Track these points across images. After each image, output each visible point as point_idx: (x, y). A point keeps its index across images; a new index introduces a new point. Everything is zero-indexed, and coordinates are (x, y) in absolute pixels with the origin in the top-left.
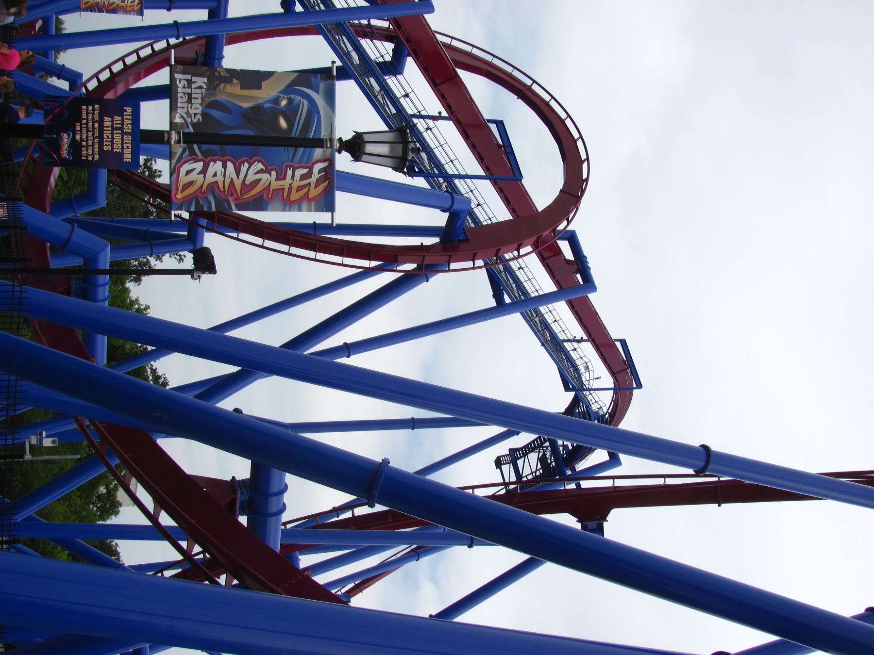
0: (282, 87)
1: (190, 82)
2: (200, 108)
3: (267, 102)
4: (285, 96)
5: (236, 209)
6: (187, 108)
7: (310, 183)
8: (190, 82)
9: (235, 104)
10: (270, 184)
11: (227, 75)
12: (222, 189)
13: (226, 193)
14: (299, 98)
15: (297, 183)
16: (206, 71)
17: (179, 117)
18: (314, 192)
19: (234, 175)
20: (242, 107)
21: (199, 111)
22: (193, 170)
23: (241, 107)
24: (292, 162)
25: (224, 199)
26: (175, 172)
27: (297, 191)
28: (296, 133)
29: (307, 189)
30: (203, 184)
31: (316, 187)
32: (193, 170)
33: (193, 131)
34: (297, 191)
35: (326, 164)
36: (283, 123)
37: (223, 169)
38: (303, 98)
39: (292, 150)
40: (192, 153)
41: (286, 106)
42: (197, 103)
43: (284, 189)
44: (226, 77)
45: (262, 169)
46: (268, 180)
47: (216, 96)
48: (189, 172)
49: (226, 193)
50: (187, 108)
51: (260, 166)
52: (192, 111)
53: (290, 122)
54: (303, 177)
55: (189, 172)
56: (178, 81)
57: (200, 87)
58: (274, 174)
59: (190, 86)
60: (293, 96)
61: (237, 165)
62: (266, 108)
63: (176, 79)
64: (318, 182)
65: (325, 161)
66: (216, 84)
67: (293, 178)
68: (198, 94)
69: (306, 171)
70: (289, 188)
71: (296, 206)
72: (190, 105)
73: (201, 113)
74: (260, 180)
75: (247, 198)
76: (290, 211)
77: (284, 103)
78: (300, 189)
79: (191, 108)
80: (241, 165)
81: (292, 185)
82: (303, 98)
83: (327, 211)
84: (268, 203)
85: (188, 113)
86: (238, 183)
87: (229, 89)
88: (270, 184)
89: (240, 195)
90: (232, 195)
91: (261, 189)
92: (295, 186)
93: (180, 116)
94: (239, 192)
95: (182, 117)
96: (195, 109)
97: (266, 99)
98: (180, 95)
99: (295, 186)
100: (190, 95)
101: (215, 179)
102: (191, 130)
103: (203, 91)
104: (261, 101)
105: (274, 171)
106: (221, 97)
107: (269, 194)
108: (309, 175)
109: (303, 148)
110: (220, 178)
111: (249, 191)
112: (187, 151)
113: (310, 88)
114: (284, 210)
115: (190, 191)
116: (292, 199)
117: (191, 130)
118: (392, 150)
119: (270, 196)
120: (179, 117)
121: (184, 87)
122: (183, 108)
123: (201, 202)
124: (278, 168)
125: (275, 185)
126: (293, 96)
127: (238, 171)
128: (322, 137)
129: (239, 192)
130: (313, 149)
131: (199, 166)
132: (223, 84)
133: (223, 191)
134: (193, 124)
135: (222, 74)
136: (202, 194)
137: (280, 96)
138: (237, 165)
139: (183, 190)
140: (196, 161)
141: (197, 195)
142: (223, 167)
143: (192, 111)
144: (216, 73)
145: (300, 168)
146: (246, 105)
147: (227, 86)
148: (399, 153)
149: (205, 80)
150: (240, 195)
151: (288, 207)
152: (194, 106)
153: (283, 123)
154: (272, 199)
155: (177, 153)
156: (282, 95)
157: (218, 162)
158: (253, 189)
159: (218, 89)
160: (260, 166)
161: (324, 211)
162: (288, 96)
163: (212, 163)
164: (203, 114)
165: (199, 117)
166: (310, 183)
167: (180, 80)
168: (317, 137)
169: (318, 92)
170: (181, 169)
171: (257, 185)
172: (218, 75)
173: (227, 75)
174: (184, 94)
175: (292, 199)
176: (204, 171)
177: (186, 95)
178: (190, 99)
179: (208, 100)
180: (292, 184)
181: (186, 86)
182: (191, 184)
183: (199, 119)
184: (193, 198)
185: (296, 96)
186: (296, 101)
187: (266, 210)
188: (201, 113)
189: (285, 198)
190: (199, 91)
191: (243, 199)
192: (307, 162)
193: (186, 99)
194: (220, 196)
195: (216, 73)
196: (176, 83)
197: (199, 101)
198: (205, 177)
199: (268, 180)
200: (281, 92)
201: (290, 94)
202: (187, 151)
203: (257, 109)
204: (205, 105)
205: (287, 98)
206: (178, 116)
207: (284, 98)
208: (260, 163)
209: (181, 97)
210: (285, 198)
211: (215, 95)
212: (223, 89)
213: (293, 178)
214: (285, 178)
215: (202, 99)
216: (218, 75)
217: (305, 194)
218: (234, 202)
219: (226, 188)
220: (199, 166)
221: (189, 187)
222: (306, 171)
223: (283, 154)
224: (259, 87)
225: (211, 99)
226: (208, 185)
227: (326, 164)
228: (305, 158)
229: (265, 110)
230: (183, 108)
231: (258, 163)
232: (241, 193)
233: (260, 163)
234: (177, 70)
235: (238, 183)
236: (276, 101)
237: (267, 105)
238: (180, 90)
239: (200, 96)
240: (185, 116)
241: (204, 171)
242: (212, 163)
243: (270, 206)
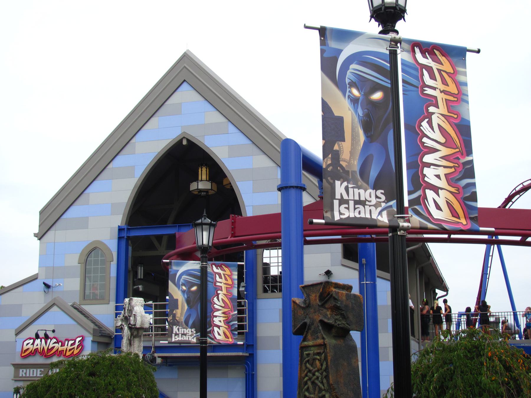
0: (339, 93)
1: (176, 334)
2: (188, 330)
3: (184, 296)
4: (348, 90)
5: (471, 155)
6: (188, 336)
7: (223, 274)
8: (176, 334)
9: (186, 312)
10: (442, 115)
11: (330, 156)
12: (453, 170)
13: (456, 165)
14: (181, 280)
15: (223, 280)
16: (328, 181)
17: (193, 339)
18: (447, 66)
19: (220, 312)
20: (187, 309)
21: (190, 330)
22: (218, 332)
23: (365, 142)
24: (418, 87)
25: (463, 168)
26: (441, 225)
27: (227, 281)
28: (197, 281)
29: (226, 276)
30: (225, 328)
31: (442, 64)
32: (218, 332)
33: (395, 201)
34: (227, 281)
35: (417, 50)
36: (194, 288)
37: (432, 167)
38: (348, 69)
39: (209, 283)
40: (210, 332)
41: (185, 286)
42: (186, 331)
43: (446, 100)
44: (332, 159)
45: (427, 122)
46: (438, 117)
47: (355, 172)
48: (219, 334)
49: (456, 165)
50: (188, 336)
51: (425, 124)
52: (190, 333)
53: (193, 285)
54: (220, 277)
55: (219, 334)
56: (176, 340)
57: (178, 329)
58: (219, 292)
59: (178, 334)
60: (181, 283)
61: (425, 150)
62: (187, 297)
63: (175, 341)
64: (223, 270)
65: (414, 52)
66: (341, 171)
67: (221, 283)
68: (182, 331)
69: (217, 276)
70: (445, 94)
71: (463, 88)
72: (367, 203)
73: (375, 190)
74: (439, 126)
75: (460, 142)
76: (467, 96)
77: (184, 288)
78: (226, 279)
79: (188, 334)
80: (426, 146)
81: (441, 90)
82: (181, 278)
83: (464, 56)
84: (463, 119)
85: (191, 336)
86: (445, 151)
87: (345, 155)
88: (442, 115)
89: (458, 150)
90: (458, 159)
91: (449, 125)
92: (225, 282)
93: (193, 339)
94: (228, 310)
95: (193, 338)
96: (189, 332)
97: (183, 297)
98: (182, 339)
99: (225, 282)
100: (182, 334)
101: (443, 177)
102: (199, 334)
103: (180, 328)
104: (184, 299)
105: (429, 109)
106: (183, 319)
107: (229, 295)
108: (430, 70)
109: (208, 278)
110: (442, 172)
111: (453, 139)
112: (416, 207)
113: (176, 274)
114: (467, 102)
115: (228, 334)
116: (231, 283)
117: (199, 334)
118: (206, 230)
119: (456, 116)
120: (193, 339)
121: (348, 208)
122: (189, 338)
123: (233, 328)
124: (426, 104)
125: (224, 291)
126: (181, 283)
127: (218, 310)
128: (388, 52)
129: (228, 310)
130: (208, 272)
131: (216, 329)
132: (176, 318)
133: (455, 169)
134: (388, 200)
135: (329, 162)
136: (459, 193)
137: (181, 290)
138: (425, 150)
139: (228, 338)
140: (213, 330)
141: (461, 198)
142: (429, 167)
143: (190, 333)
144: (171, 321)
145: (216, 279)
146: (186, 307)
147: (342, 157)
148: (208, 227)
149: (174, 327)
150: (458, 150)
151: (464, 97)
152: (188, 332)
153: (194, 288)
154: (458, 114)
155: (420, 222)
156: (180, 289)
157: (214, 320)
158: (227, 303)
159: (179, 321)
160: (425, 124)
161: (465, 60)
162: (348, 86)
163: (214, 323)
164: (191, 328)
165: (193, 330)
166: (438, 69)
167: (340, 214)
168: (200, 271)
169: (178, 271)
170: (435, 217)
171: (224, 300)
172: (172, 321)
173: (330, 156)
174: (182, 337)
175: (231, 283)
176: (219, 327)
177: (356, 206)
178: (359, 202)
179: (185, 326)
180: (440, 89)
181: (178, 336)
182: (224, 333)
183: (194, 330)
184: (464, 202)
185: (347, 77)
186: (353, 78)
187: (469, 122)
188: (375, 190)
189: (456, 99)
190: (180, 330)
191: (460, 146)
192: (417, 70)
193: (184, 336)
194: (460, 172)
195: (171, 321)
196: (345, 218)
197: (185, 330)
198: (221, 326)
199: (438, 117)
200: (179, 289)
201: (180, 285)
202: (416, 207)
203: (188, 302)
204: (187, 327)
205: (181, 286)
206: (192, 340)
207: (350, 92)
208: (422, 124)
209: (184, 338)
210: (456, 99)
211: (182, 322)
212: (346, 162)
213: (221, 283)
214: (221, 287)
215: (184, 328)
216: (172, 321)
217: (229, 277)
218: (233, 312)
219: (451, 164)
220: (216, 329)
221: (226, 334)
222: (217, 276)
223: (210, 286)
224: (177, 300)
225: (184, 324)
226: (449, 185)
227: (417, 50)
228: (413, 72)
229: (188, 297)
230: (189, 338)
231: (214, 299)
232: (455, 149)
233: (422, 124)
234: (170, 340)
235: (445, 151)
236: (183, 292)
237: (186, 296)
238: (180, 339)
239: (356, 190)
240: (193, 337)
241: (436, 189)
242: (214, 323)
243: (466, 118)
